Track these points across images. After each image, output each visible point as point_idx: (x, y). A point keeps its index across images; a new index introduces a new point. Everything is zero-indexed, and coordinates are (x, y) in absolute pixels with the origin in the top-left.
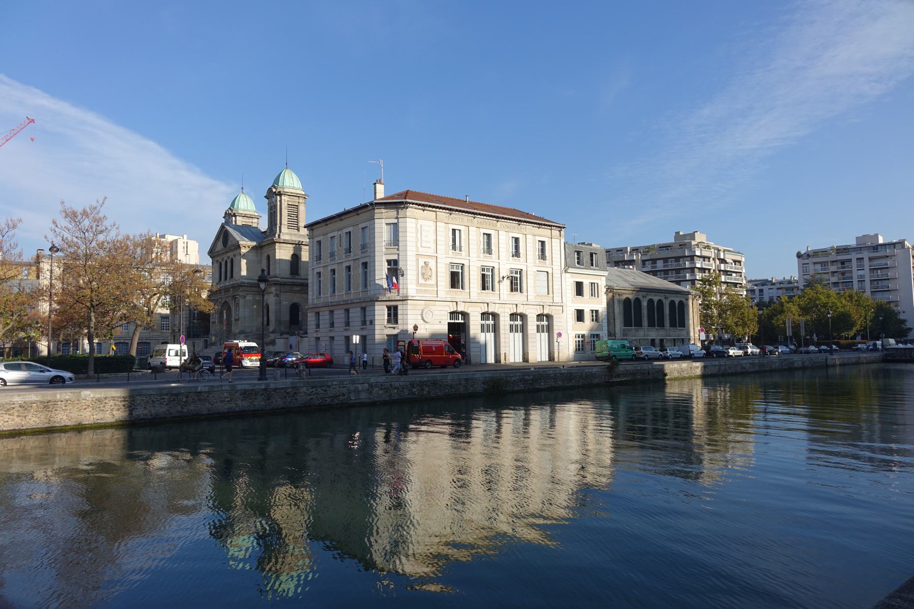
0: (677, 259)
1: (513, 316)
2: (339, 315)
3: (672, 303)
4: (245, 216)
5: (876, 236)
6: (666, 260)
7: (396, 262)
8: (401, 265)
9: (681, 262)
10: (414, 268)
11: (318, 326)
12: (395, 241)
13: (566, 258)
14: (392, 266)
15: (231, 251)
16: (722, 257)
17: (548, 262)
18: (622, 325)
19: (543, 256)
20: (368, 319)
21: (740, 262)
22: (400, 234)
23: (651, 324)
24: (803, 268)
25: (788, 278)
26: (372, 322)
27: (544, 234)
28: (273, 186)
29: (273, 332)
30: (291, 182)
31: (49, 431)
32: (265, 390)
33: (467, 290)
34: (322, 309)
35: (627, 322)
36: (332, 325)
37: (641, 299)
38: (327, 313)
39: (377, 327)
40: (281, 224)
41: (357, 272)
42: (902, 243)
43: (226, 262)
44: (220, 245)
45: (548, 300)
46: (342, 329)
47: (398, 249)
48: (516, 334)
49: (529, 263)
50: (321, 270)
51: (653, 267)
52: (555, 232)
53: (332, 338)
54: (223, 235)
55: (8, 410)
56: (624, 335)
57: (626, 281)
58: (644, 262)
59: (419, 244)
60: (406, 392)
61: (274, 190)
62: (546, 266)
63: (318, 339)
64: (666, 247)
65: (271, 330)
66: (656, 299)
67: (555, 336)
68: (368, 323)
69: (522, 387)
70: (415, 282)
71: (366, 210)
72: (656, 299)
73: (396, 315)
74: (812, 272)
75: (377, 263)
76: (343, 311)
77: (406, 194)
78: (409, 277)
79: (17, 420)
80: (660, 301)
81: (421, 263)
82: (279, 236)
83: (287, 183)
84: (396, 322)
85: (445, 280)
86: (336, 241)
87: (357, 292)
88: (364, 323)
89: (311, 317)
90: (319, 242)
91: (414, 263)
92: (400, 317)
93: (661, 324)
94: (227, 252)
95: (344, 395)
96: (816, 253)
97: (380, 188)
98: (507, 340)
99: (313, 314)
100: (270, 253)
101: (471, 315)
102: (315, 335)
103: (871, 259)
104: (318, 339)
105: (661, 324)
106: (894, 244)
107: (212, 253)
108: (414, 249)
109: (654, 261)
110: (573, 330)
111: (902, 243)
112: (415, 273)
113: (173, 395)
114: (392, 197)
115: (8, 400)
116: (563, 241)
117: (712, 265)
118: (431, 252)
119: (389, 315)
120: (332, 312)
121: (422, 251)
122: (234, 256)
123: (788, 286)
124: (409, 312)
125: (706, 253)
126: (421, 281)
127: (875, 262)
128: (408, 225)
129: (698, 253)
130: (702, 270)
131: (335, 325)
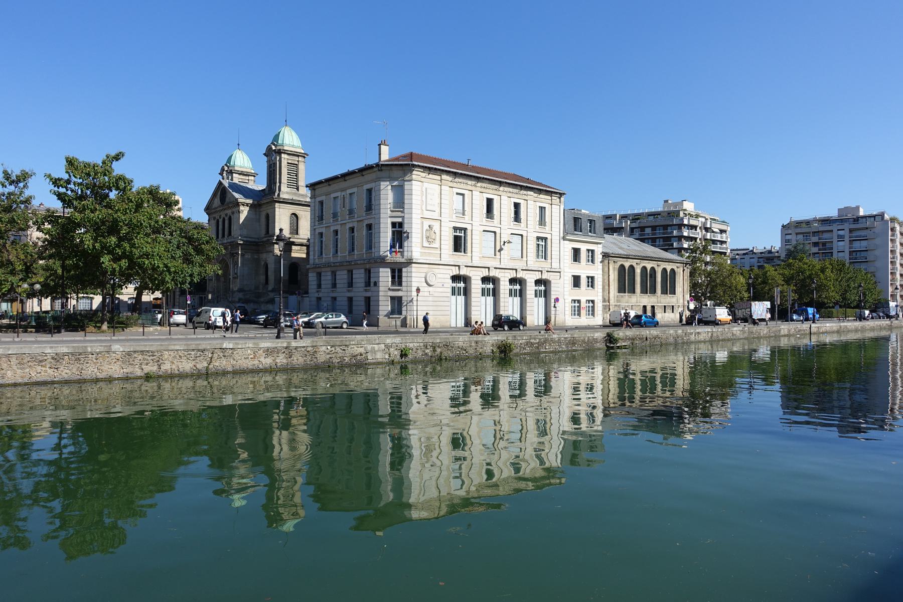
0: (665, 227)
1: (485, 280)
2: (342, 276)
3: (644, 268)
4: (241, 173)
5: (858, 208)
6: (654, 228)
7: (401, 225)
8: (406, 228)
9: (669, 231)
10: (420, 231)
11: (319, 286)
12: (400, 203)
13: (564, 225)
14: (397, 229)
15: (229, 208)
16: (708, 226)
17: (548, 228)
18: (616, 290)
19: (517, 218)
20: (372, 280)
21: (725, 231)
22: (406, 197)
23: (644, 291)
24: (785, 242)
25: (768, 248)
26: (376, 284)
27: (518, 196)
28: (273, 143)
29: (272, 291)
30: (290, 139)
31: (81, 382)
32: (286, 348)
33: (469, 254)
34: (323, 270)
35: (621, 289)
36: (334, 285)
37: (635, 266)
38: (329, 273)
39: (381, 289)
40: (280, 182)
41: (361, 234)
42: (882, 215)
43: (224, 220)
44: (217, 201)
45: (519, 265)
46: (345, 290)
47: (403, 212)
48: (459, 297)
49: (476, 222)
50: (323, 230)
51: (641, 235)
52: (555, 199)
53: (334, 299)
54: (221, 192)
55: (41, 361)
56: (618, 301)
57: (621, 248)
58: (632, 229)
59: (424, 208)
60: (420, 353)
61: (274, 148)
62: (493, 225)
63: (319, 299)
64: (654, 214)
65: (270, 288)
66: (627, 264)
67: (553, 301)
68: (372, 284)
69: (528, 350)
70: (419, 245)
71: (379, 170)
72: (627, 264)
73: (400, 277)
74: (794, 243)
75: (382, 225)
76: (346, 272)
77: (411, 156)
78: (414, 240)
79: (50, 371)
80: (653, 269)
81: (426, 227)
82: (279, 195)
83: (286, 141)
84: (400, 284)
85: (449, 243)
86: (339, 202)
87: (360, 252)
88: (368, 284)
89: (312, 277)
90: (321, 203)
91: (419, 226)
92: (404, 279)
93: (653, 291)
94: (224, 209)
95: (361, 355)
96: (799, 224)
97: (385, 149)
98: (506, 304)
99: (315, 274)
100: (269, 212)
101: (473, 278)
102: (316, 295)
103: (851, 231)
104: (319, 299)
105: (653, 291)
106: (874, 216)
107: (208, 209)
108: (419, 212)
109: (642, 229)
110: (570, 295)
111: (882, 215)
112: (420, 236)
113: (199, 350)
114: (397, 159)
115: (39, 351)
116: (562, 207)
117: (699, 234)
118: (436, 215)
119: (393, 277)
120: (334, 274)
121: (427, 214)
122: (233, 213)
123: (768, 257)
124: (413, 274)
125: (693, 222)
126: (426, 244)
127: (854, 234)
128: (414, 187)
129: (686, 222)
130: (689, 239)
131: (338, 286)
